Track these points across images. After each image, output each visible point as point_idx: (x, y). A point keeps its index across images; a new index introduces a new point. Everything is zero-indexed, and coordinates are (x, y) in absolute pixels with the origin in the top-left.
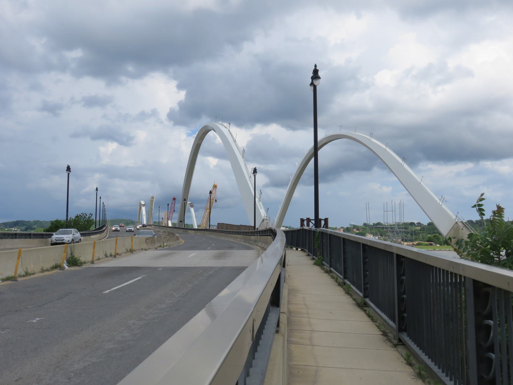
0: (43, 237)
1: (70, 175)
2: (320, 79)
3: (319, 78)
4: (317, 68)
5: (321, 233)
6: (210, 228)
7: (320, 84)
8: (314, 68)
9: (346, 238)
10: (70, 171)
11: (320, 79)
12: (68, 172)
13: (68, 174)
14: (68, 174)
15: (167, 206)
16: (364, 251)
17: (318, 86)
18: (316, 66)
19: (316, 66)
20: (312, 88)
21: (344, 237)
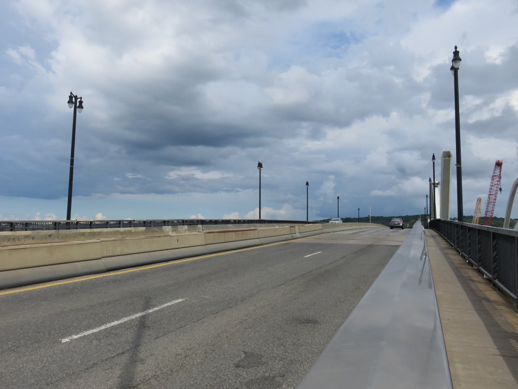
0: (168, 224)
1: (308, 188)
2: (461, 60)
3: (460, 60)
4: (434, 155)
5: (456, 225)
6: (261, 218)
7: (461, 65)
8: (433, 155)
9: (496, 232)
10: (308, 185)
11: (461, 60)
12: (307, 186)
13: (307, 187)
14: (307, 187)
15: (306, 187)
16: (479, 234)
17: (460, 66)
18: (434, 154)
19: (434, 154)
20: (453, 72)
21: (494, 231)
